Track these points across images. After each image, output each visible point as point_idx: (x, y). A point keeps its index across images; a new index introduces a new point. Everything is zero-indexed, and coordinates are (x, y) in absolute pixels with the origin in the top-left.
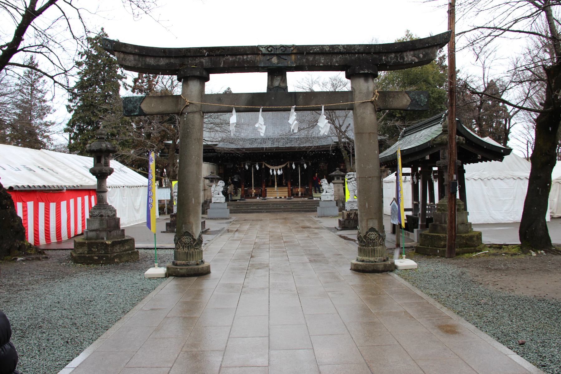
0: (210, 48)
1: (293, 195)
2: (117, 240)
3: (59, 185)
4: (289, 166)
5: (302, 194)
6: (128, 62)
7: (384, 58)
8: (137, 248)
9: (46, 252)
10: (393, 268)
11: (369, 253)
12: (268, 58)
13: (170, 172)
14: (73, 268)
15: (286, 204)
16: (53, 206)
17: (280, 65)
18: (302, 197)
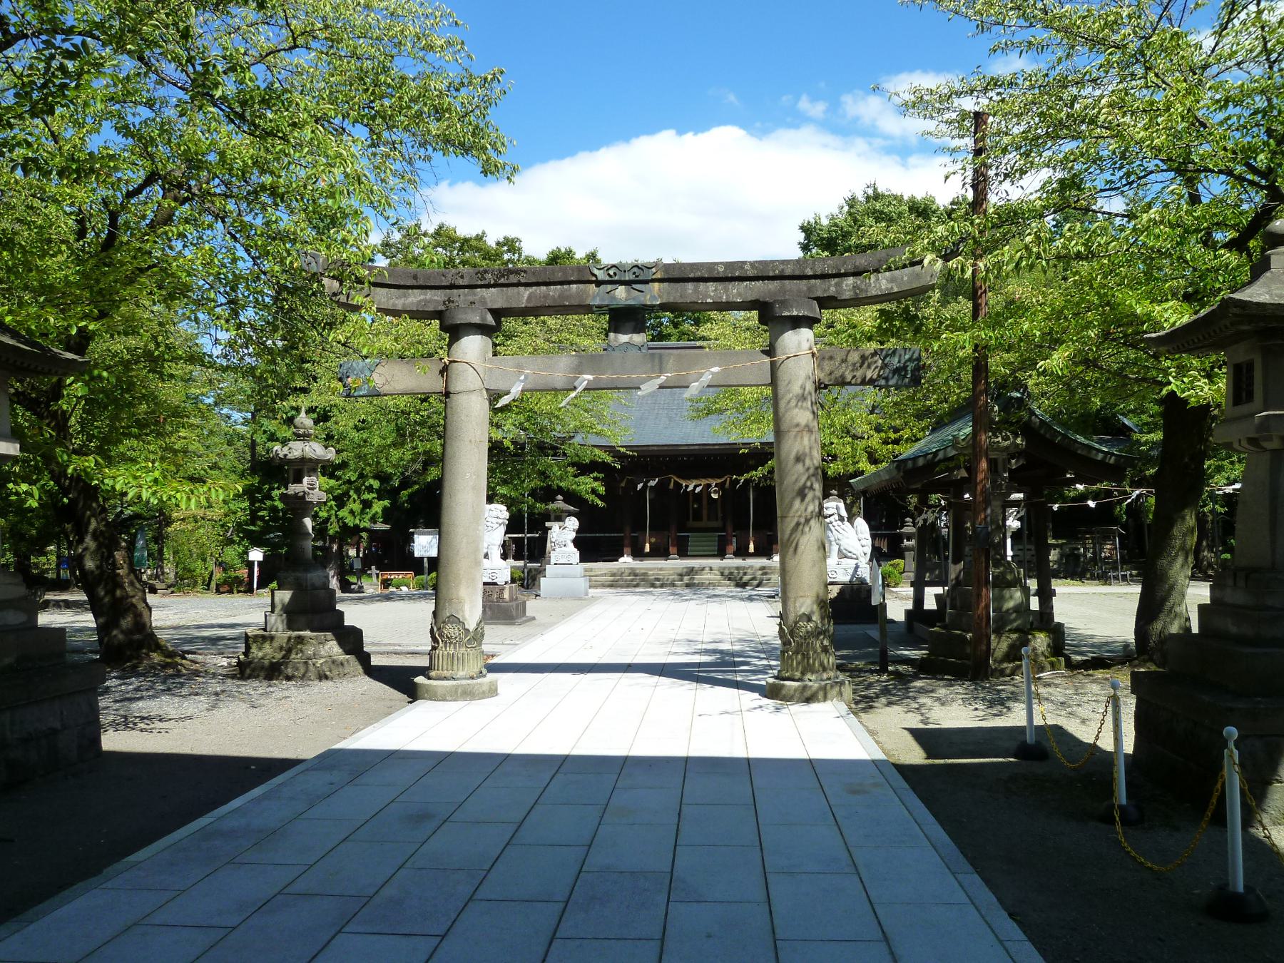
12: (609, 287)
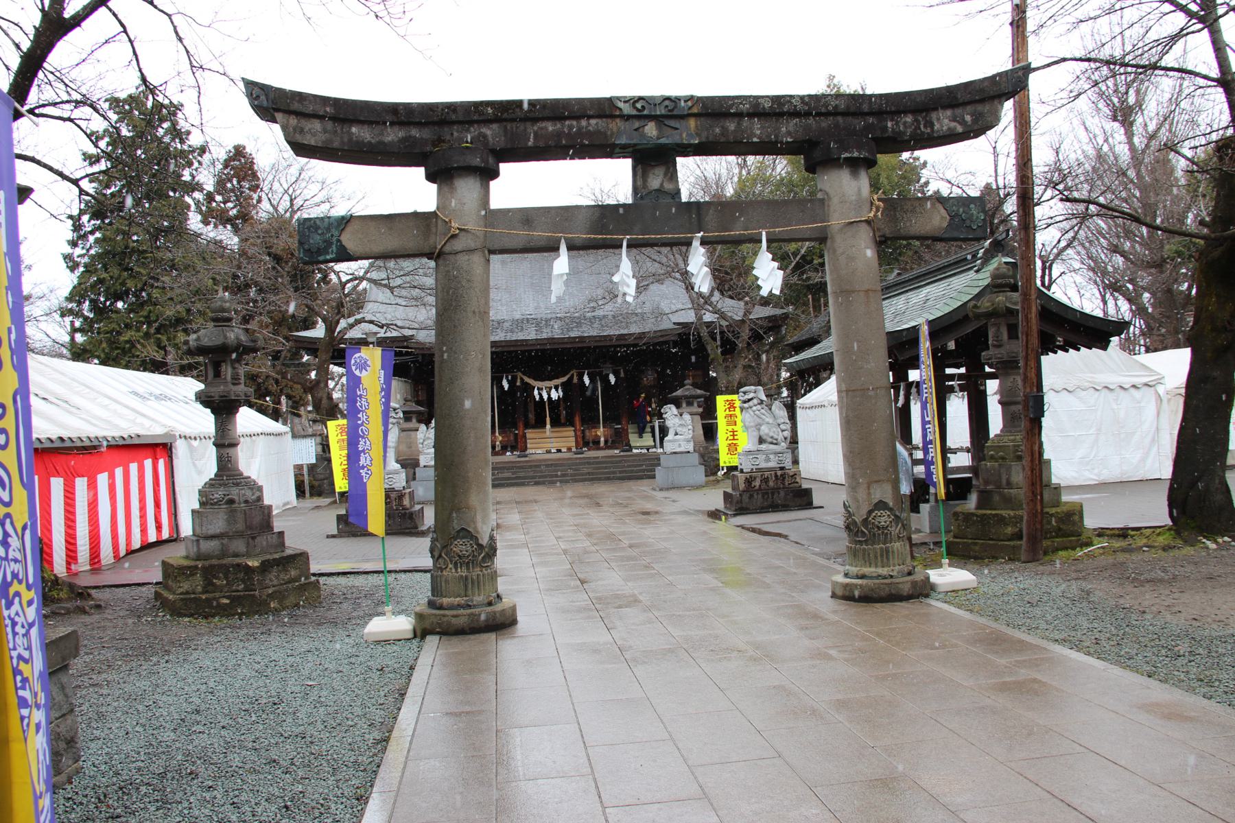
0: (501, 102)
1: (586, 444)
2: (269, 557)
3: (92, 436)
4: (575, 380)
5: (606, 442)
6: (308, 136)
7: (889, 124)
8: (314, 575)
9: (93, 592)
10: (924, 590)
11: (876, 557)
12: (637, 124)
13: (321, 400)
14: (183, 628)
15: (577, 464)
16: (81, 484)
17: (663, 141)
18: (607, 447)
